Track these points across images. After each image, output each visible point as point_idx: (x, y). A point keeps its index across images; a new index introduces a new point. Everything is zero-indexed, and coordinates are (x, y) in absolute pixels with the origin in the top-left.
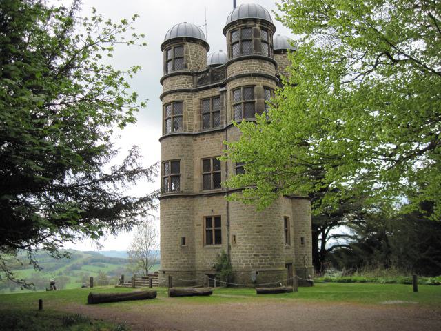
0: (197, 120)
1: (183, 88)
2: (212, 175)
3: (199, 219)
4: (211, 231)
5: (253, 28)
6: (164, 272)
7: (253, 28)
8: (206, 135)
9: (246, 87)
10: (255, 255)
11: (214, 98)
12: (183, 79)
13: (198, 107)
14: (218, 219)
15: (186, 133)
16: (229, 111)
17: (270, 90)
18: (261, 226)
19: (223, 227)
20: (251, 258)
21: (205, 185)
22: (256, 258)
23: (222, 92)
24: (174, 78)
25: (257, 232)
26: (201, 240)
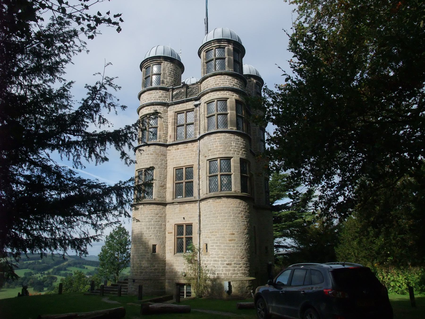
0: (172, 132)
1: (159, 101)
2: (184, 183)
3: (170, 228)
4: (183, 238)
5: (226, 47)
6: (134, 281)
7: (226, 47)
8: (180, 145)
9: (219, 100)
10: (228, 264)
11: (188, 111)
12: (160, 93)
13: (172, 119)
14: (189, 226)
15: (161, 143)
16: (202, 123)
17: (241, 105)
18: (234, 234)
19: (195, 235)
20: (223, 267)
21: (177, 192)
22: (229, 267)
23: (196, 106)
24: (151, 92)
25: (230, 240)
26: (172, 248)
